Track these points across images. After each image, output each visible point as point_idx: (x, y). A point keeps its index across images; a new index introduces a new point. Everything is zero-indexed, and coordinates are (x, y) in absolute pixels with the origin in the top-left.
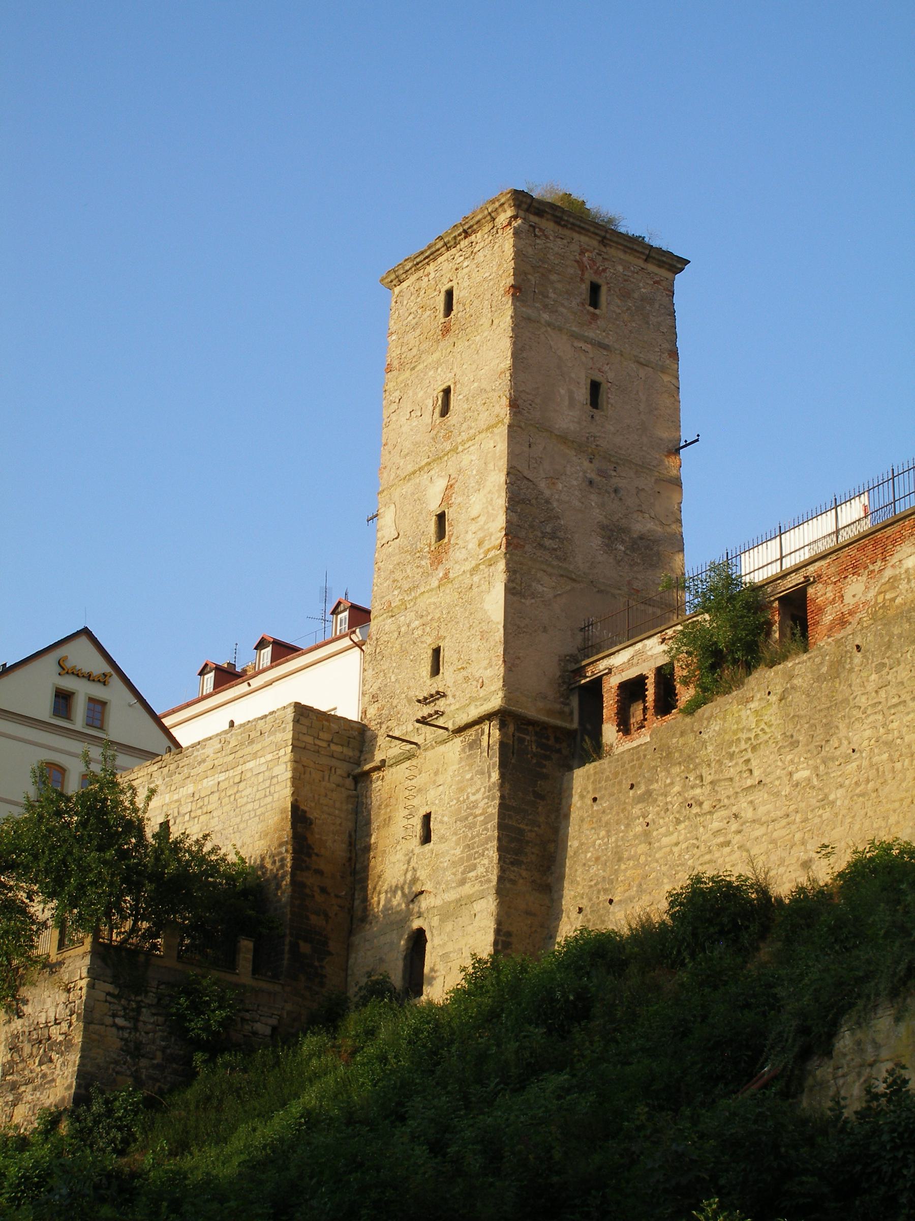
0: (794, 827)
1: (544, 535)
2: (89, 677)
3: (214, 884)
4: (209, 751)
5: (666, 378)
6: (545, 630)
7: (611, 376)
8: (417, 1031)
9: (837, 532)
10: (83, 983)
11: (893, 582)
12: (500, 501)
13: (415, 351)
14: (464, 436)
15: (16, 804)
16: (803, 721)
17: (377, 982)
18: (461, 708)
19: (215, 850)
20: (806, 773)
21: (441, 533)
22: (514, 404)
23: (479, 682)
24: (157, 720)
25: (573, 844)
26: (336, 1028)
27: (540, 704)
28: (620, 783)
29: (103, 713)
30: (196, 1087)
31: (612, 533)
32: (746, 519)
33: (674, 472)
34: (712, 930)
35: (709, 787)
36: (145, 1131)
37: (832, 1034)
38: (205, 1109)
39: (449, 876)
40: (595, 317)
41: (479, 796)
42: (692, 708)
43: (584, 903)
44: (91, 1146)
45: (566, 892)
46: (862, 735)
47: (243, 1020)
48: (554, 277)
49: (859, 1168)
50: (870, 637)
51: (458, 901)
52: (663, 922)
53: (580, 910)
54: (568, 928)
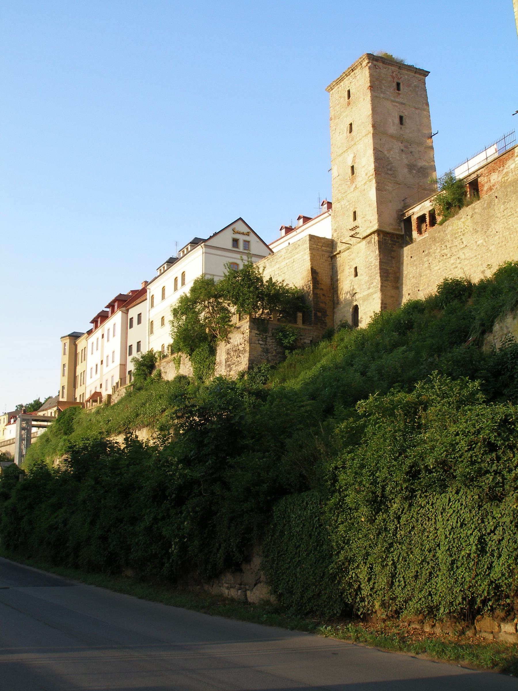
0: (478, 260)
1: (388, 169)
2: (243, 234)
3: (287, 296)
4: (283, 253)
5: (425, 113)
6: (390, 202)
7: (406, 114)
8: (357, 338)
9: (487, 158)
10: (248, 331)
11: (507, 174)
12: (372, 159)
13: (339, 112)
14: (358, 139)
15: (221, 276)
16: (479, 224)
17: (344, 323)
18: (363, 232)
19: (287, 285)
20: (481, 241)
21: (353, 173)
22: (374, 126)
23: (369, 221)
24: (267, 246)
25: (405, 273)
26: (331, 339)
27: (391, 227)
28: (419, 251)
29: (249, 245)
30: (287, 361)
31: (411, 167)
32: (454, 158)
33: (431, 144)
34: (452, 296)
35: (449, 249)
36: (271, 376)
37: (492, 326)
38: (290, 368)
39: (364, 287)
40: (399, 94)
41: (372, 259)
42: (441, 224)
43: (410, 292)
44: (255, 382)
45: (404, 289)
46: (499, 226)
47: (301, 339)
48: (384, 82)
49: (500, 367)
50: (500, 193)
51: (368, 294)
52: (436, 295)
53: (409, 294)
54: (405, 300)
